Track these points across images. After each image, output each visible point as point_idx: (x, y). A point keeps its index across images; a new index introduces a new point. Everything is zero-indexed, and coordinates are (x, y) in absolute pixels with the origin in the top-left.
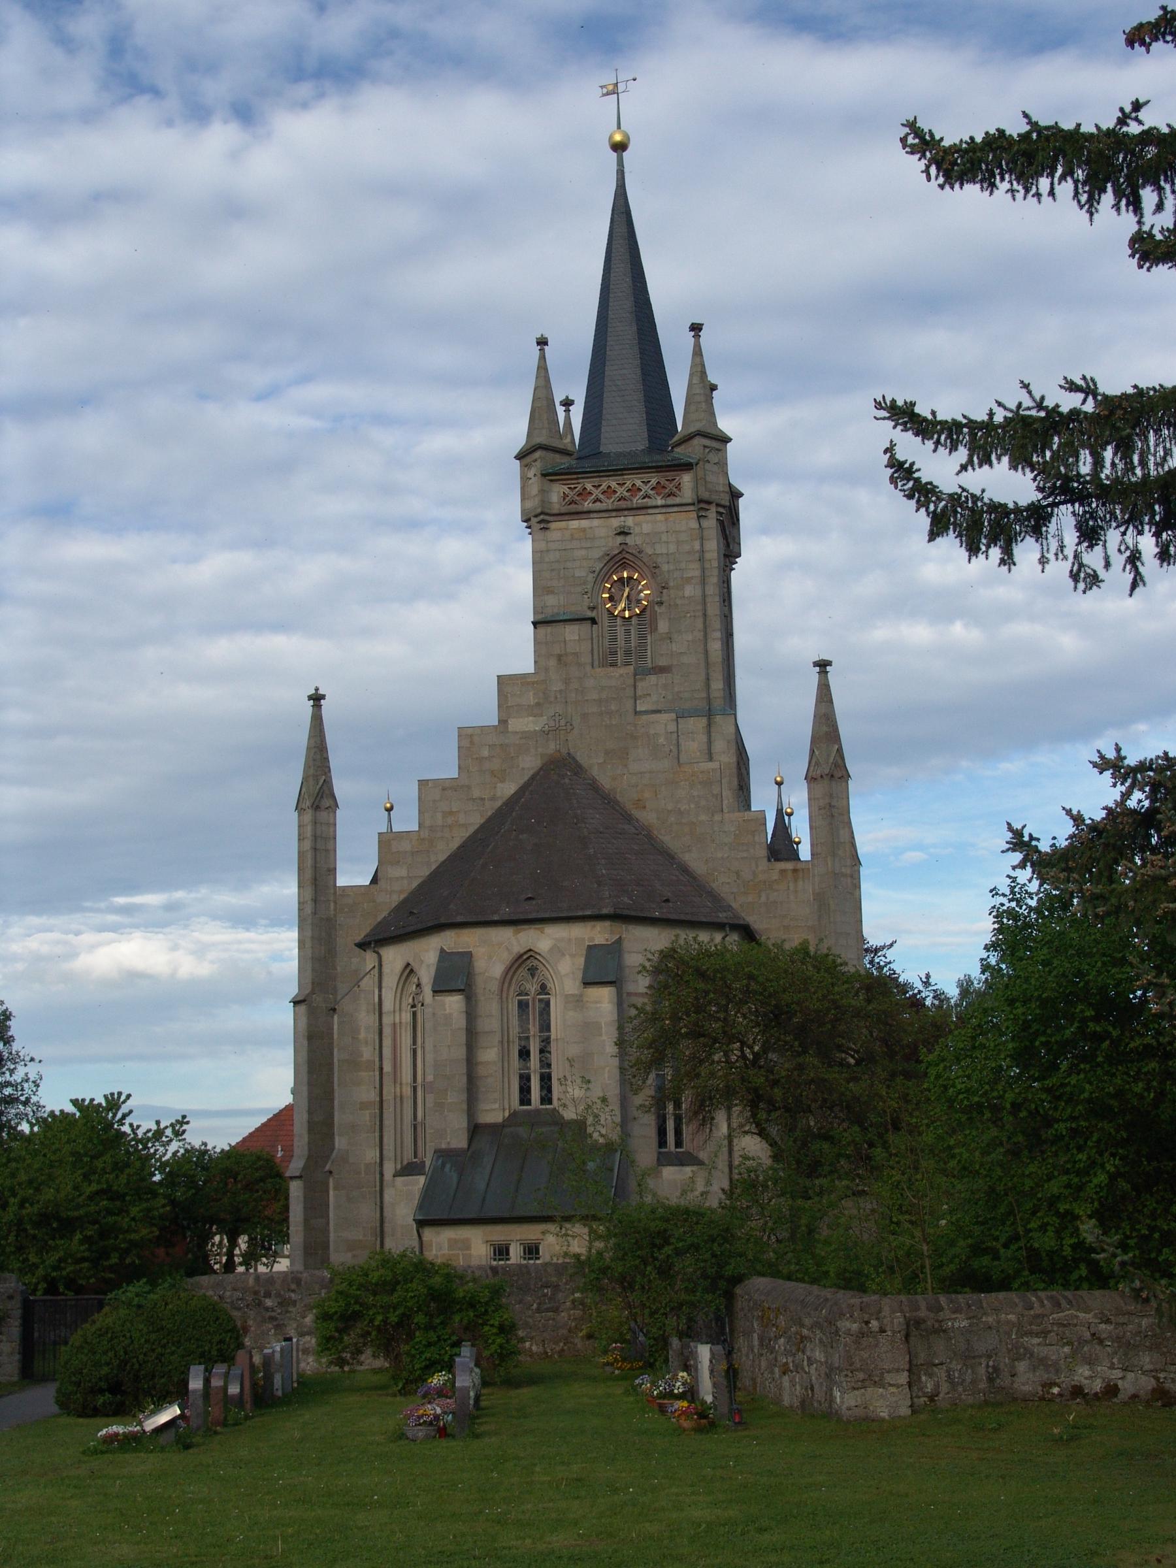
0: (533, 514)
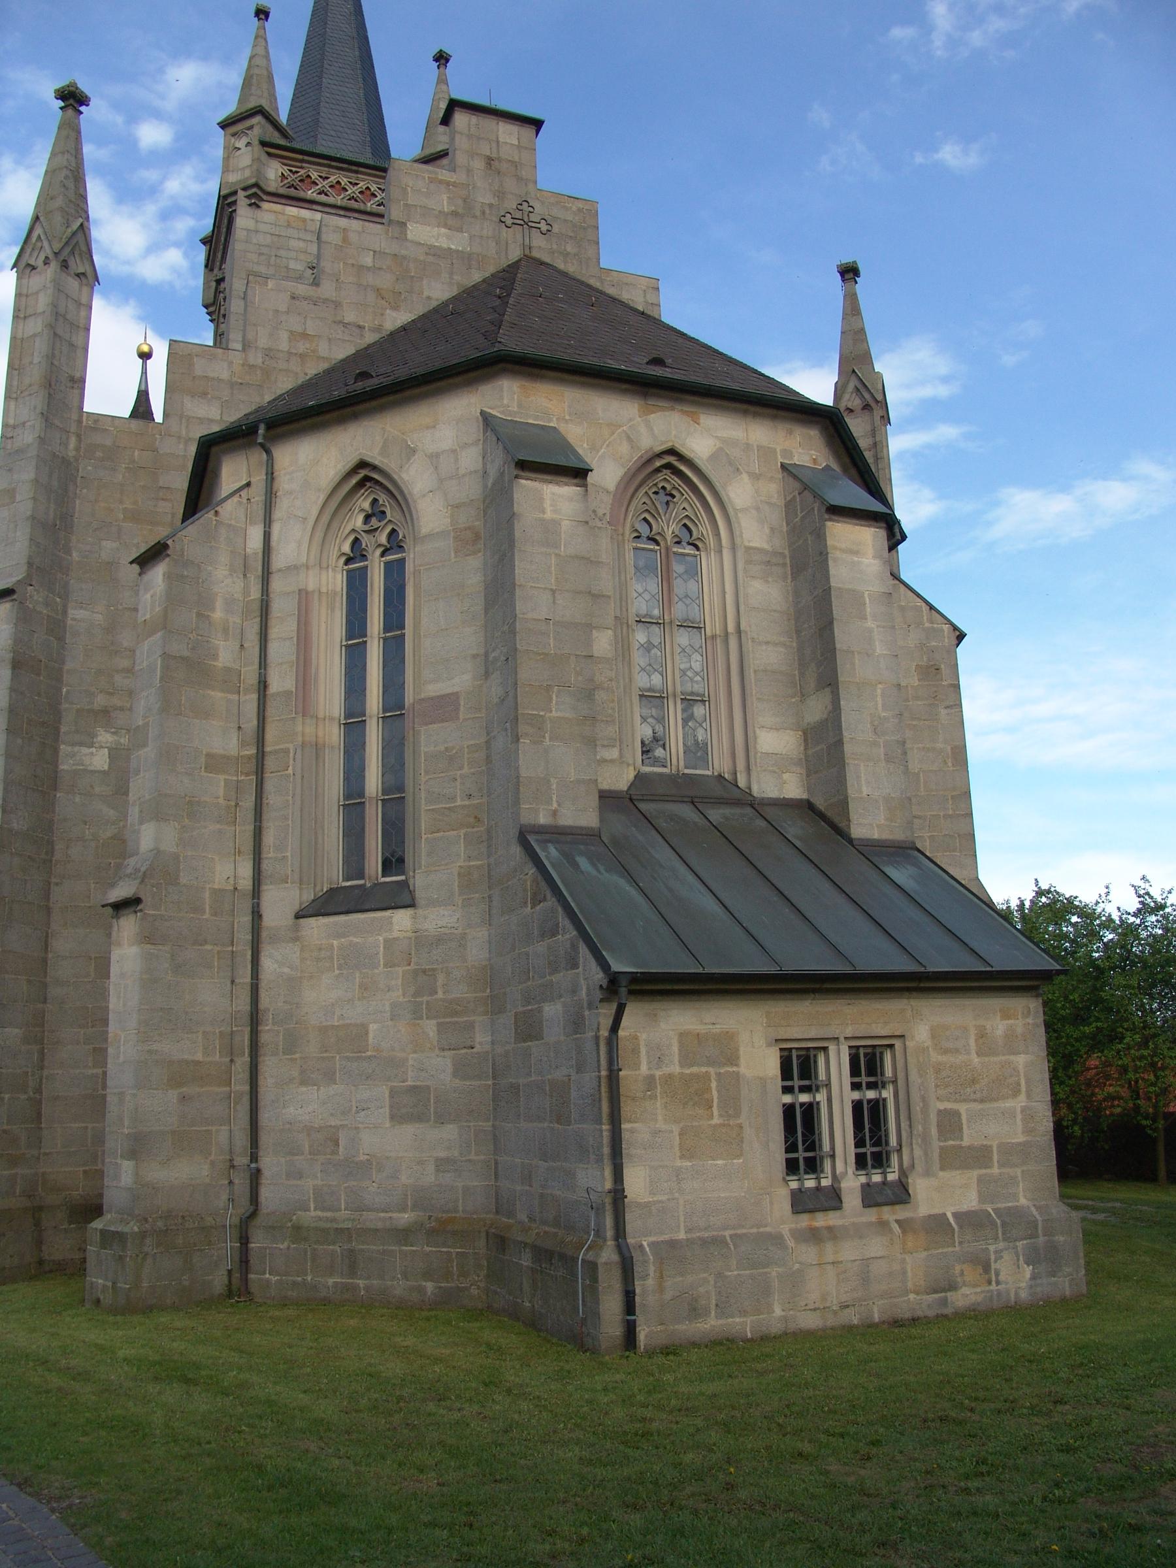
0: (242, 186)
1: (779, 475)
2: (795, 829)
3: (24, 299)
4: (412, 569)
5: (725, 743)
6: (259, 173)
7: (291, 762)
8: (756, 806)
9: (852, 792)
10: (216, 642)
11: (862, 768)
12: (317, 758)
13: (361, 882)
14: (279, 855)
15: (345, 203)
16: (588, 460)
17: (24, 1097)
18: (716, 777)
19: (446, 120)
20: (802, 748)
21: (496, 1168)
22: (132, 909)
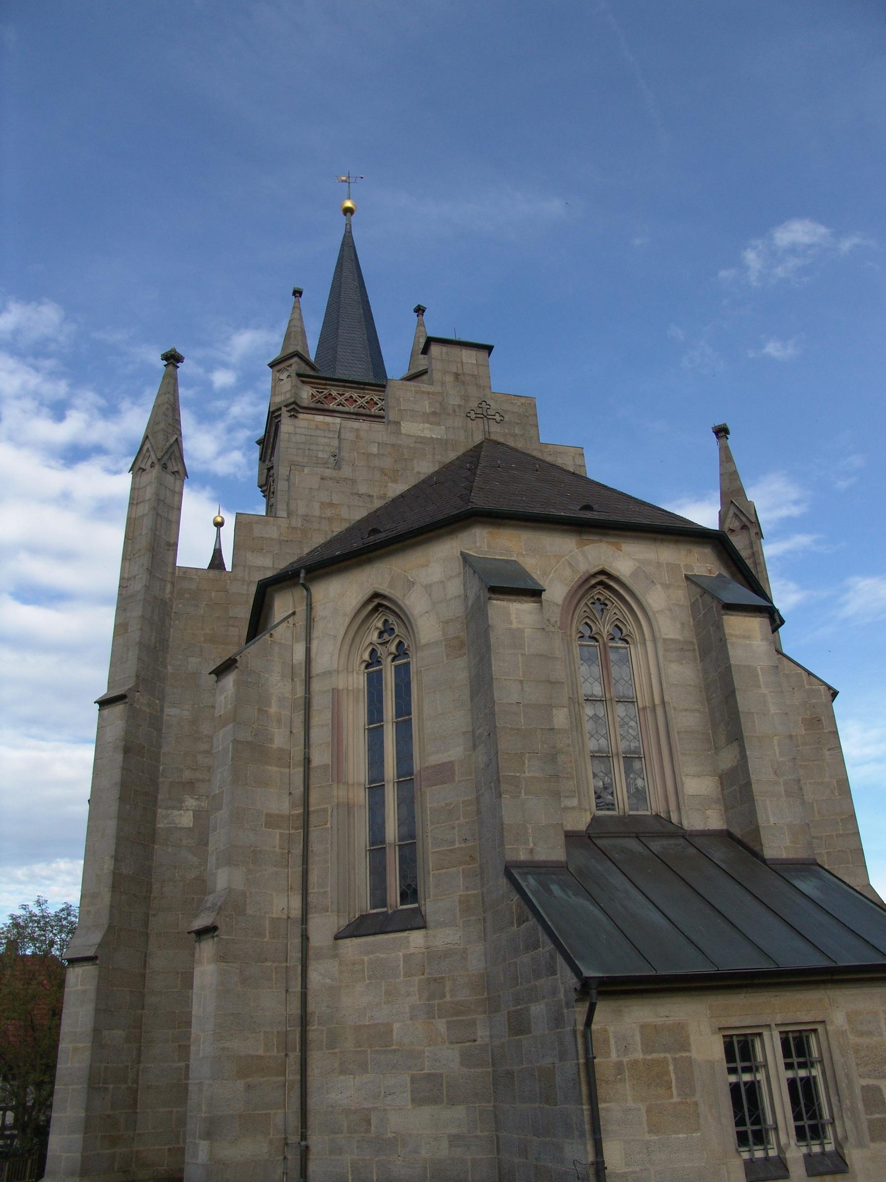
1: (684, 584)
2: (719, 854)
3: (136, 491)
4: (415, 670)
5: (659, 790)
6: (296, 394)
7: (329, 818)
8: (687, 836)
9: (761, 822)
10: (272, 730)
11: (768, 802)
12: (349, 814)
13: (384, 910)
14: (322, 890)
15: (356, 410)
16: (541, 583)
17: (123, 1086)
18: (654, 816)
19: (425, 351)
20: (719, 789)
21: (498, 1143)
22: (210, 935)
